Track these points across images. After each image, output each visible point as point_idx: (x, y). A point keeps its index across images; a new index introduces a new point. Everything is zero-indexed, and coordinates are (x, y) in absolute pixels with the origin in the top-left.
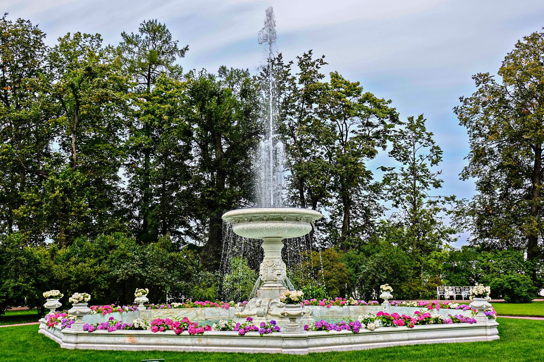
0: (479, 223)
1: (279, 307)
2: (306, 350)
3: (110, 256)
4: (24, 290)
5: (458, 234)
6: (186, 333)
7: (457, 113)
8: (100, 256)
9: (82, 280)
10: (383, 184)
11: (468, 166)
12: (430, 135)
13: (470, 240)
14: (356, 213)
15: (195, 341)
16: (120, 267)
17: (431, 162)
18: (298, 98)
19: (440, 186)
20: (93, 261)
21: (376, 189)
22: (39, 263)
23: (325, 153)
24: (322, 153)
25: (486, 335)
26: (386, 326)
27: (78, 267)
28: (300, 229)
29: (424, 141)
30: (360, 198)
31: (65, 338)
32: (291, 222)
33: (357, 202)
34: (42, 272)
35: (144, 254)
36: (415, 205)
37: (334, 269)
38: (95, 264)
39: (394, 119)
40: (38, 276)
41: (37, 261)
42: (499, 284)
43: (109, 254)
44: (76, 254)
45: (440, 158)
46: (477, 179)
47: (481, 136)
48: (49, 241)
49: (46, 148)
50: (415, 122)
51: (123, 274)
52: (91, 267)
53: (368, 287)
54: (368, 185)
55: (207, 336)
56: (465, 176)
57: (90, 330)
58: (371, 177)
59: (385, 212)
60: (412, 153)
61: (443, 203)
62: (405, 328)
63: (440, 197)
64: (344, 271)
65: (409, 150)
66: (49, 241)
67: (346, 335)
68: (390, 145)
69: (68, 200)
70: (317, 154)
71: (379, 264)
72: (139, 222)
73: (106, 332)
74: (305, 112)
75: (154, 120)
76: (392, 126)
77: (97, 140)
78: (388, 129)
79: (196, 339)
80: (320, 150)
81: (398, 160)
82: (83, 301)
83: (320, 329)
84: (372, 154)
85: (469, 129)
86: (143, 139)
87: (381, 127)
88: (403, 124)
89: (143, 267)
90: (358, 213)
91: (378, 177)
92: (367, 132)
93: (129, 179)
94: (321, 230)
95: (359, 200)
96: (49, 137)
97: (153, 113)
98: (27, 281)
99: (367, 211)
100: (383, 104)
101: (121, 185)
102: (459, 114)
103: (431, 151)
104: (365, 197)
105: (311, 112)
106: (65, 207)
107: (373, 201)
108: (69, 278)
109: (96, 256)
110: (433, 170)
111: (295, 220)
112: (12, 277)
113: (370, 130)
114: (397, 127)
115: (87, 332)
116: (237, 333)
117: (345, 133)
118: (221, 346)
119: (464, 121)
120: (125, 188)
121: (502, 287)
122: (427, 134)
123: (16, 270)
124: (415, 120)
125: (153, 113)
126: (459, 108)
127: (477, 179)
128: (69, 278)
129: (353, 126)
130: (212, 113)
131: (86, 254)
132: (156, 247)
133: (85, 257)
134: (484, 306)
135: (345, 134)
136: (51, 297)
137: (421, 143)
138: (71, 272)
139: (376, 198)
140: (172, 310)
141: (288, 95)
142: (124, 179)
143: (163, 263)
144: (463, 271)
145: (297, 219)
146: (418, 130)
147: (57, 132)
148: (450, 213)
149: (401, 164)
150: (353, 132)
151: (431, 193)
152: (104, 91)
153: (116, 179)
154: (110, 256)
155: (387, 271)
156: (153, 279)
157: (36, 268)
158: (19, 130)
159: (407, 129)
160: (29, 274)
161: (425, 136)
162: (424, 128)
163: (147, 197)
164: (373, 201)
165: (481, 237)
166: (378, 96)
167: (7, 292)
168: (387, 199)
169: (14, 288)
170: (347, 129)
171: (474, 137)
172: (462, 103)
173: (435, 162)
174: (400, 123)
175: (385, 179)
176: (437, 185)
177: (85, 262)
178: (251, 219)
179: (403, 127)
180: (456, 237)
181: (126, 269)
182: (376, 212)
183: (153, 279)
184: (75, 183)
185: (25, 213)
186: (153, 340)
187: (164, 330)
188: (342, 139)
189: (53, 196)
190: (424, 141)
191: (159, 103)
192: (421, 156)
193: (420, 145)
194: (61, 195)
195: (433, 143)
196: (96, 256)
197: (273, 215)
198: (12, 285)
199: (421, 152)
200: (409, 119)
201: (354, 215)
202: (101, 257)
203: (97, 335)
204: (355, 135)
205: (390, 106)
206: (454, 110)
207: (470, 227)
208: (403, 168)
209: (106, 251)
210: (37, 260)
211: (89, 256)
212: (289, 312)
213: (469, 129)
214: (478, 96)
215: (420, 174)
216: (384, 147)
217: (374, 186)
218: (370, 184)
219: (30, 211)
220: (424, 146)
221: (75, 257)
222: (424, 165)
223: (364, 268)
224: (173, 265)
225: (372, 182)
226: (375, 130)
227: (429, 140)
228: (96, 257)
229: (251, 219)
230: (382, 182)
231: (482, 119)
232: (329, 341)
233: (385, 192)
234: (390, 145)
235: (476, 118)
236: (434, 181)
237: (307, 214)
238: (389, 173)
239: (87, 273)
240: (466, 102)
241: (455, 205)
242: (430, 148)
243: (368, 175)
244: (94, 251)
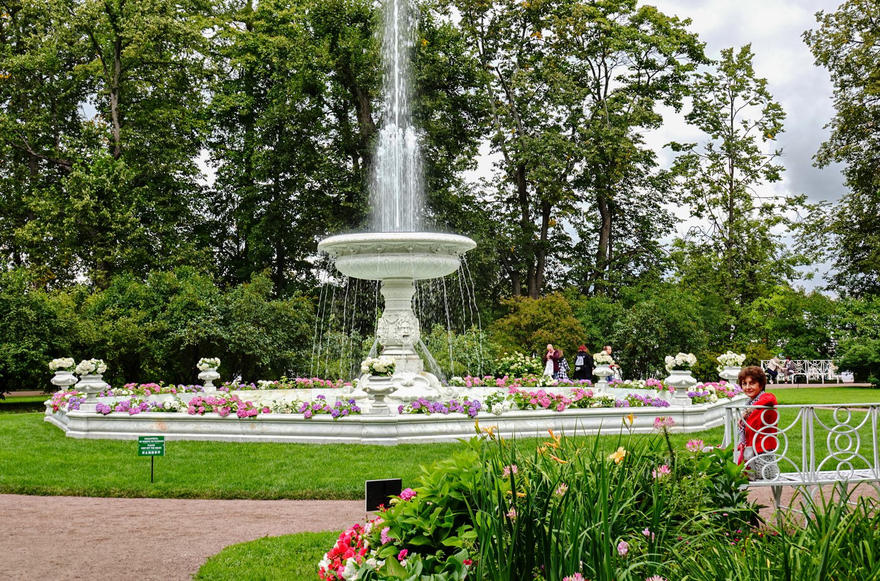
0: (851, 248)
1: (405, 386)
2: (395, 439)
3: (169, 306)
4: (32, 361)
5: (814, 266)
6: (234, 416)
7: (809, 43)
8: (153, 306)
9: (124, 345)
10: (675, 174)
11: (829, 141)
12: (763, 82)
13: (830, 276)
14: (624, 228)
15: (247, 427)
16: (185, 325)
17: (762, 133)
18: (515, 20)
19: (777, 177)
20: (142, 314)
21: (662, 182)
22: (55, 317)
23: (564, 120)
24: (559, 120)
25: (683, 425)
26: (524, 409)
27: (119, 323)
28: (436, 266)
29: (752, 95)
30: (632, 200)
31: (71, 424)
32: (421, 255)
33: (626, 207)
34: (60, 332)
35: (227, 303)
36: (734, 214)
37: (559, 329)
38: (146, 319)
39: (697, 55)
40: (53, 338)
41: (52, 315)
42: (861, 356)
43: (169, 302)
44: (114, 302)
45: (780, 125)
46: (845, 165)
47: (857, 85)
48: (82, 278)
49: (74, 116)
50: (735, 59)
51: (190, 336)
52: (140, 323)
53: (626, 360)
54: (646, 177)
55: (262, 421)
56: (823, 159)
57: (104, 414)
58: (652, 162)
59: (677, 225)
60: (729, 118)
61: (784, 208)
62: (550, 412)
63: (777, 198)
64: (576, 332)
65: (723, 111)
66: (82, 278)
67: (458, 420)
68: (688, 103)
69: (105, 212)
70: (551, 122)
71: (645, 321)
72: (238, 244)
73: (126, 415)
74: (529, 45)
75: (256, 64)
76: (690, 67)
77: (155, 103)
78: (682, 74)
79: (247, 425)
80: (555, 114)
81: (704, 130)
82: (95, 372)
83: (420, 412)
84: (655, 121)
85: (833, 72)
86: (240, 99)
87: (668, 71)
88: (713, 63)
89: (225, 323)
90: (629, 227)
91: (665, 161)
92: (646, 79)
93: (216, 170)
94: (562, 259)
95: (631, 204)
96: (78, 96)
97: (254, 51)
98: (37, 346)
99: (645, 223)
100: (677, 25)
101: (201, 182)
102: (813, 44)
103: (765, 112)
104: (642, 199)
105: (539, 45)
106: (100, 223)
107: (655, 206)
108: (104, 341)
109: (148, 306)
110: (766, 148)
111: (428, 252)
112: (12, 341)
113: (651, 74)
114: (701, 69)
115: (100, 415)
116: (301, 417)
117: (603, 81)
118: (281, 434)
119: (824, 58)
120: (210, 186)
121: (865, 361)
122: (756, 81)
123: (18, 329)
124: (734, 55)
125: (254, 51)
126: (814, 34)
127: (845, 165)
128: (104, 341)
129: (618, 71)
130: (349, 54)
131: (133, 303)
132: (246, 291)
133: (129, 308)
134: (684, 383)
135: (604, 83)
136: (61, 369)
137: (746, 98)
138: (106, 332)
139: (661, 200)
140: (256, 393)
141: (498, 13)
142: (206, 170)
143: (258, 317)
144: (809, 332)
145: (432, 249)
146: (740, 73)
147: (91, 86)
148: (793, 228)
149: (707, 137)
150: (619, 78)
151: (761, 191)
152: (163, 21)
153: (194, 170)
154: (169, 306)
155: (658, 333)
156: (240, 345)
157: (50, 326)
158: (23, 88)
159: (722, 73)
160: (38, 335)
161: (752, 84)
162: (752, 70)
163: (249, 204)
164: (655, 206)
165: (852, 270)
166: (667, 9)
167: (5, 363)
168: (681, 202)
169: (15, 356)
170: (606, 75)
171: (843, 86)
172: (821, 23)
173: (769, 134)
174: (707, 62)
175: (678, 165)
176: (773, 176)
177: (129, 316)
178: (359, 250)
179: (712, 70)
180: (811, 271)
181: (194, 328)
182: (661, 226)
183: (240, 345)
184: (116, 181)
185: (35, 234)
186: (190, 427)
187: (203, 413)
188: (598, 93)
189: (79, 205)
190: (752, 95)
191: (264, 32)
192: (746, 122)
193: (744, 103)
194: (93, 203)
195: (769, 98)
196: (148, 306)
197: (393, 243)
198: (12, 351)
199: (745, 115)
200: (724, 54)
201: (622, 232)
202: (156, 308)
203: (115, 419)
204: (625, 85)
205: (689, 30)
206: (803, 38)
207: (829, 253)
208: (711, 146)
209: (163, 298)
210: (50, 313)
211: (137, 306)
212: (372, 387)
213: (833, 72)
214: (849, 10)
215: (744, 155)
216: (678, 107)
217: (657, 179)
218: (650, 174)
219: (43, 232)
220: (752, 104)
221: (114, 308)
222: (751, 139)
223: (619, 327)
224: (276, 321)
225: (654, 172)
226: (658, 75)
227: (761, 92)
228: (148, 308)
229: (359, 250)
230: (670, 171)
231: (858, 53)
232: (430, 428)
233: (678, 189)
234: (688, 103)
235: (845, 52)
236: (767, 169)
237: (446, 242)
238: (686, 153)
239: (132, 333)
240: (827, 22)
241: (805, 213)
242: (764, 106)
243: (648, 158)
244: (146, 299)
